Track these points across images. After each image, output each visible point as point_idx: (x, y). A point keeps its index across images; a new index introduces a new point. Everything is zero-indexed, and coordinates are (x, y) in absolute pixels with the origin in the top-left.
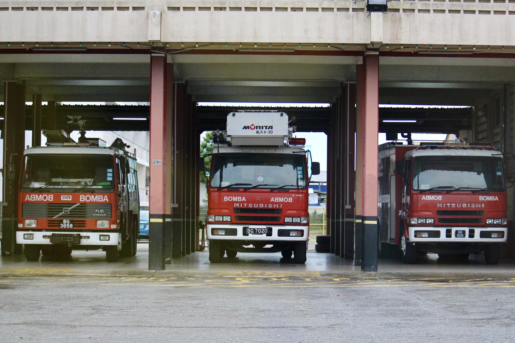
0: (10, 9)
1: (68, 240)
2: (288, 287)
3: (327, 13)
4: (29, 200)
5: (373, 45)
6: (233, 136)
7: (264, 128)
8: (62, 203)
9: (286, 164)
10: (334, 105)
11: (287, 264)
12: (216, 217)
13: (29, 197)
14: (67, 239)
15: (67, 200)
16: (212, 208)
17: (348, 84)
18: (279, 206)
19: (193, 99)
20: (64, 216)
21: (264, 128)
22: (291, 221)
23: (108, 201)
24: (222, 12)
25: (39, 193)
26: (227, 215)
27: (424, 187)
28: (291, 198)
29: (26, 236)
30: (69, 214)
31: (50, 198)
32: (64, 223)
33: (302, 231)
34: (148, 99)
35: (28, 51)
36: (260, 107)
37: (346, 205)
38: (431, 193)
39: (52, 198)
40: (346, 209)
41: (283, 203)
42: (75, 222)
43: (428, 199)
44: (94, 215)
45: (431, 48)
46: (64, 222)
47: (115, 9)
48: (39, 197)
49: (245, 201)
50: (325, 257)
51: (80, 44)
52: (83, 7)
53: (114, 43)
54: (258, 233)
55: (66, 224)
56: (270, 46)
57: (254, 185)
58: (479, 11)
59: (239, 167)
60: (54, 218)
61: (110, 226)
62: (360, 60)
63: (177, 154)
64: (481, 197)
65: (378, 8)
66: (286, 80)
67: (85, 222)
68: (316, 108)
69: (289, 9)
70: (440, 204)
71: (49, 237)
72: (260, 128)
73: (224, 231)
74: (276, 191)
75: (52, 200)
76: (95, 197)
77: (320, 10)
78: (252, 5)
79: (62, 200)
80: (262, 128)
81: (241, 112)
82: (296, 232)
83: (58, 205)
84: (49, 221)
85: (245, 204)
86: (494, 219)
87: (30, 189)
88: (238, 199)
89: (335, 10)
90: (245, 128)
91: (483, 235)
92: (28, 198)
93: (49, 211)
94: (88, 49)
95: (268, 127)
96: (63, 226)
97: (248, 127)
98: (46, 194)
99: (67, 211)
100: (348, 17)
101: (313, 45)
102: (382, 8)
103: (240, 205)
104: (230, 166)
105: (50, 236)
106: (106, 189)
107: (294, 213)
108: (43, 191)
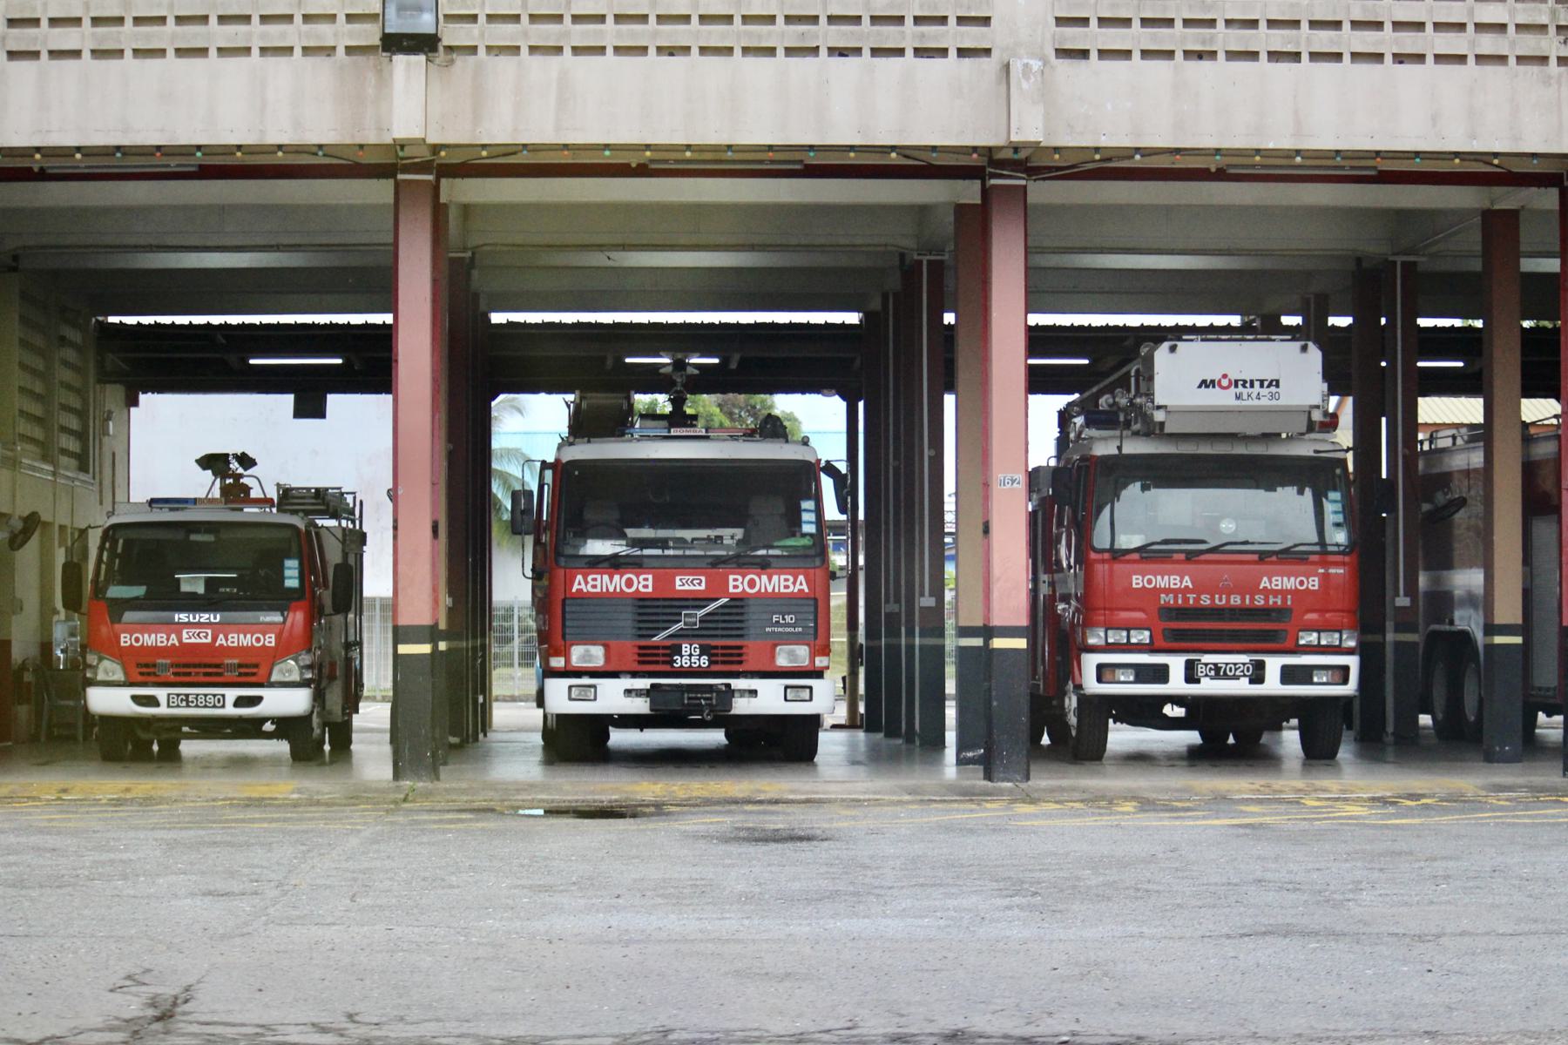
0: (128, 53)
1: (703, 702)
2: (1524, 823)
3: (1490, 70)
4: (585, 590)
5: (402, 147)
6: (1172, 406)
7: (1257, 384)
8: (676, 596)
9: (1283, 485)
10: (869, 316)
11: (1250, 762)
12: (1110, 633)
13: (582, 582)
14: (699, 699)
15: (692, 588)
16: (1099, 609)
17: (925, 263)
18: (1284, 600)
19: (483, 307)
20: (681, 635)
21: (1257, 384)
22: (1125, 641)
23: (807, 590)
24: (1205, 64)
25: (612, 570)
26: (1140, 628)
27: (1129, 540)
28: (1316, 579)
29: (575, 692)
30: (700, 629)
31: (644, 583)
32: (683, 653)
33: (1345, 670)
34: (391, 306)
35: (633, 169)
36: (1060, 326)
37: (922, 594)
38: (1142, 558)
39: (650, 583)
40: (921, 608)
41: (1295, 592)
42: (715, 651)
43: (1277, 585)
44: (768, 629)
45: (1097, 157)
46: (684, 649)
47: (909, 53)
48: (611, 580)
49: (1191, 586)
50: (1285, 744)
51: (850, 151)
52: (818, 47)
53: (880, 150)
54: (1226, 677)
55: (691, 655)
56: (1339, 159)
57: (1213, 544)
58: (1099, 51)
59: (1154, 491)
60: (655, 639)
61: (812, 661)
62: (969, 192)
63: (930, 457)
64: (735, 580)
65: (412, 43)
66: (1228, 253)
67: (744, 650)
68: (827, 325)
69: (1388, 58)
70: (1167, 596)
71: (639, 693)
72: (1244, 386)
73: (1133, 671)
74: (1274, 558)
75: (650, 589)
76: (770, 580)
77: (1471, 60)
78: (1289, 46)
79: (678, 588)
80: (1252, 386)
81: (1192, 340)
82: (1330, 672)
83: (667, 603)
84: (640, 647)
85: (1192, 596)
86: (1319, 632)
87: (587, 560)
88: (1171, 582)
89: (1512, 61)
90: (1204, 384)
91: (1289, 675)
92: (580, 584)
93: (640, 621)
94: (807, 166)
95: (1266, 384)
96: (681, 662)
97: (1213, 382)
98: (754, 573)
99: (688, 620)
100: (1547, 81)
101: (1413, 155)
102: (424, 44)
103: (1176, 598)
104: (1134, 488)
105: (648, 690)
106: (795, 556)
107: (1141, 620)
108: (625, 564)
